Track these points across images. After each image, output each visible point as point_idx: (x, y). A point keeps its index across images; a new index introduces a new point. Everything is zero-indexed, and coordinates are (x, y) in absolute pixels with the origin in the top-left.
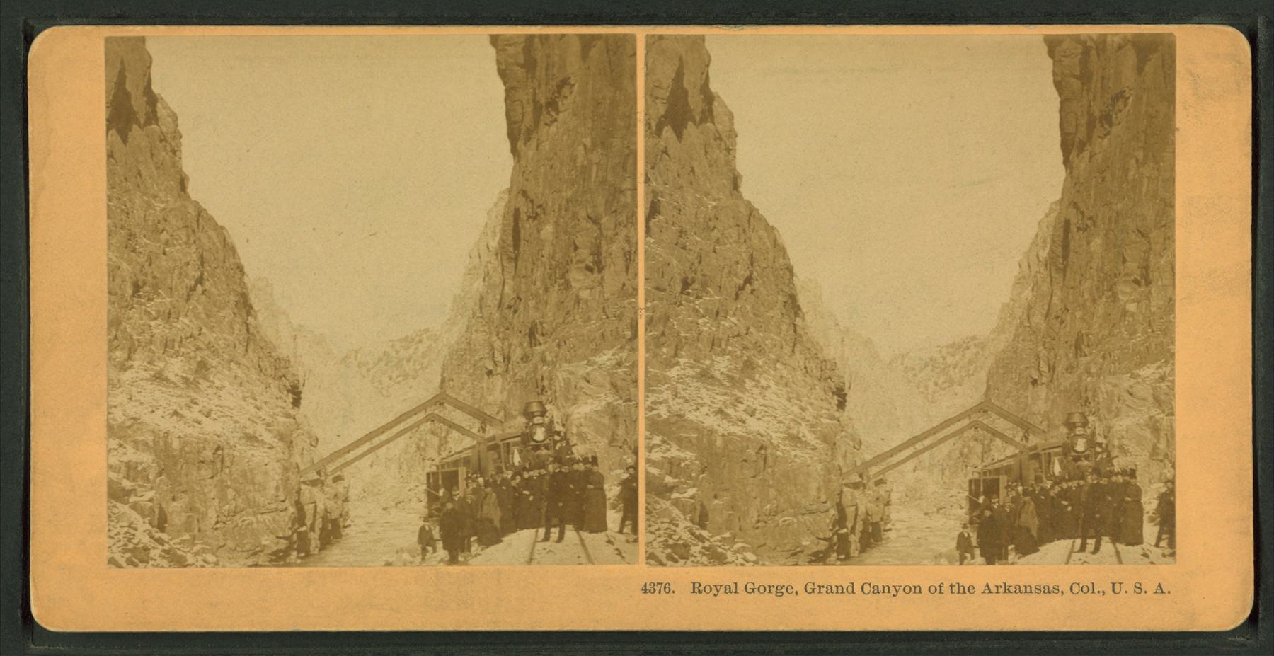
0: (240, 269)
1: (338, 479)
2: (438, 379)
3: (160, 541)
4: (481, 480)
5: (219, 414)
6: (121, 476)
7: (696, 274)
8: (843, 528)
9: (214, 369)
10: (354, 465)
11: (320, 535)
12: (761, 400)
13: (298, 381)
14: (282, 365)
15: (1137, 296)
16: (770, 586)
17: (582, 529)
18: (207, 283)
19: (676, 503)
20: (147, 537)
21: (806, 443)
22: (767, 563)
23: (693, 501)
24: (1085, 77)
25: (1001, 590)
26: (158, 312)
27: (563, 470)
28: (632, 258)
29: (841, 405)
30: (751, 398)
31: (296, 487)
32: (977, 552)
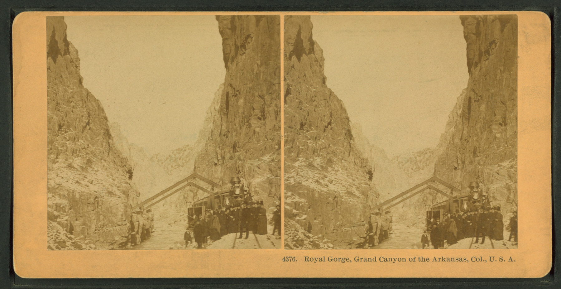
0: (106, 118)
1: (149, 211)
2: (193, 167)
3: (308, 237)
4: (212, 211)
5: (97, 182)
6: (53, 210)
7: (306, 120)
8: (371, 233)
9: (94, 163)
10: (156, 205)
11: (141, 236)
12: (335, 176)
13: (372, 169)
14: (365, 162)
15: (501, 131)
16: (339, 258)
17: (256, 233)
18: (91, 124)
19: (298, 222)
20: (65, 237)
21: (355, 195)
22: (338, 248)
23: (305, 221)
24: (478, 34)
25: (441, 260)
26: (70, 137)
27: (248, 207)
28: (278, 114)
29: (370, 178)
30: (331, 176)
31: (130, 214)
32: (430, 243)
